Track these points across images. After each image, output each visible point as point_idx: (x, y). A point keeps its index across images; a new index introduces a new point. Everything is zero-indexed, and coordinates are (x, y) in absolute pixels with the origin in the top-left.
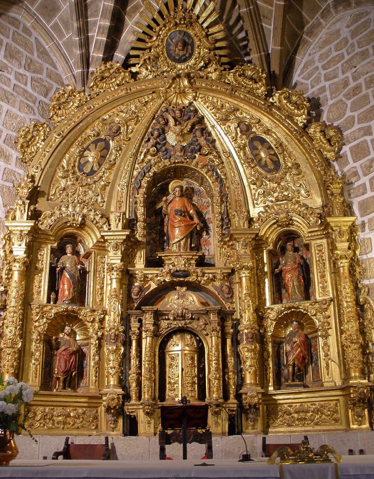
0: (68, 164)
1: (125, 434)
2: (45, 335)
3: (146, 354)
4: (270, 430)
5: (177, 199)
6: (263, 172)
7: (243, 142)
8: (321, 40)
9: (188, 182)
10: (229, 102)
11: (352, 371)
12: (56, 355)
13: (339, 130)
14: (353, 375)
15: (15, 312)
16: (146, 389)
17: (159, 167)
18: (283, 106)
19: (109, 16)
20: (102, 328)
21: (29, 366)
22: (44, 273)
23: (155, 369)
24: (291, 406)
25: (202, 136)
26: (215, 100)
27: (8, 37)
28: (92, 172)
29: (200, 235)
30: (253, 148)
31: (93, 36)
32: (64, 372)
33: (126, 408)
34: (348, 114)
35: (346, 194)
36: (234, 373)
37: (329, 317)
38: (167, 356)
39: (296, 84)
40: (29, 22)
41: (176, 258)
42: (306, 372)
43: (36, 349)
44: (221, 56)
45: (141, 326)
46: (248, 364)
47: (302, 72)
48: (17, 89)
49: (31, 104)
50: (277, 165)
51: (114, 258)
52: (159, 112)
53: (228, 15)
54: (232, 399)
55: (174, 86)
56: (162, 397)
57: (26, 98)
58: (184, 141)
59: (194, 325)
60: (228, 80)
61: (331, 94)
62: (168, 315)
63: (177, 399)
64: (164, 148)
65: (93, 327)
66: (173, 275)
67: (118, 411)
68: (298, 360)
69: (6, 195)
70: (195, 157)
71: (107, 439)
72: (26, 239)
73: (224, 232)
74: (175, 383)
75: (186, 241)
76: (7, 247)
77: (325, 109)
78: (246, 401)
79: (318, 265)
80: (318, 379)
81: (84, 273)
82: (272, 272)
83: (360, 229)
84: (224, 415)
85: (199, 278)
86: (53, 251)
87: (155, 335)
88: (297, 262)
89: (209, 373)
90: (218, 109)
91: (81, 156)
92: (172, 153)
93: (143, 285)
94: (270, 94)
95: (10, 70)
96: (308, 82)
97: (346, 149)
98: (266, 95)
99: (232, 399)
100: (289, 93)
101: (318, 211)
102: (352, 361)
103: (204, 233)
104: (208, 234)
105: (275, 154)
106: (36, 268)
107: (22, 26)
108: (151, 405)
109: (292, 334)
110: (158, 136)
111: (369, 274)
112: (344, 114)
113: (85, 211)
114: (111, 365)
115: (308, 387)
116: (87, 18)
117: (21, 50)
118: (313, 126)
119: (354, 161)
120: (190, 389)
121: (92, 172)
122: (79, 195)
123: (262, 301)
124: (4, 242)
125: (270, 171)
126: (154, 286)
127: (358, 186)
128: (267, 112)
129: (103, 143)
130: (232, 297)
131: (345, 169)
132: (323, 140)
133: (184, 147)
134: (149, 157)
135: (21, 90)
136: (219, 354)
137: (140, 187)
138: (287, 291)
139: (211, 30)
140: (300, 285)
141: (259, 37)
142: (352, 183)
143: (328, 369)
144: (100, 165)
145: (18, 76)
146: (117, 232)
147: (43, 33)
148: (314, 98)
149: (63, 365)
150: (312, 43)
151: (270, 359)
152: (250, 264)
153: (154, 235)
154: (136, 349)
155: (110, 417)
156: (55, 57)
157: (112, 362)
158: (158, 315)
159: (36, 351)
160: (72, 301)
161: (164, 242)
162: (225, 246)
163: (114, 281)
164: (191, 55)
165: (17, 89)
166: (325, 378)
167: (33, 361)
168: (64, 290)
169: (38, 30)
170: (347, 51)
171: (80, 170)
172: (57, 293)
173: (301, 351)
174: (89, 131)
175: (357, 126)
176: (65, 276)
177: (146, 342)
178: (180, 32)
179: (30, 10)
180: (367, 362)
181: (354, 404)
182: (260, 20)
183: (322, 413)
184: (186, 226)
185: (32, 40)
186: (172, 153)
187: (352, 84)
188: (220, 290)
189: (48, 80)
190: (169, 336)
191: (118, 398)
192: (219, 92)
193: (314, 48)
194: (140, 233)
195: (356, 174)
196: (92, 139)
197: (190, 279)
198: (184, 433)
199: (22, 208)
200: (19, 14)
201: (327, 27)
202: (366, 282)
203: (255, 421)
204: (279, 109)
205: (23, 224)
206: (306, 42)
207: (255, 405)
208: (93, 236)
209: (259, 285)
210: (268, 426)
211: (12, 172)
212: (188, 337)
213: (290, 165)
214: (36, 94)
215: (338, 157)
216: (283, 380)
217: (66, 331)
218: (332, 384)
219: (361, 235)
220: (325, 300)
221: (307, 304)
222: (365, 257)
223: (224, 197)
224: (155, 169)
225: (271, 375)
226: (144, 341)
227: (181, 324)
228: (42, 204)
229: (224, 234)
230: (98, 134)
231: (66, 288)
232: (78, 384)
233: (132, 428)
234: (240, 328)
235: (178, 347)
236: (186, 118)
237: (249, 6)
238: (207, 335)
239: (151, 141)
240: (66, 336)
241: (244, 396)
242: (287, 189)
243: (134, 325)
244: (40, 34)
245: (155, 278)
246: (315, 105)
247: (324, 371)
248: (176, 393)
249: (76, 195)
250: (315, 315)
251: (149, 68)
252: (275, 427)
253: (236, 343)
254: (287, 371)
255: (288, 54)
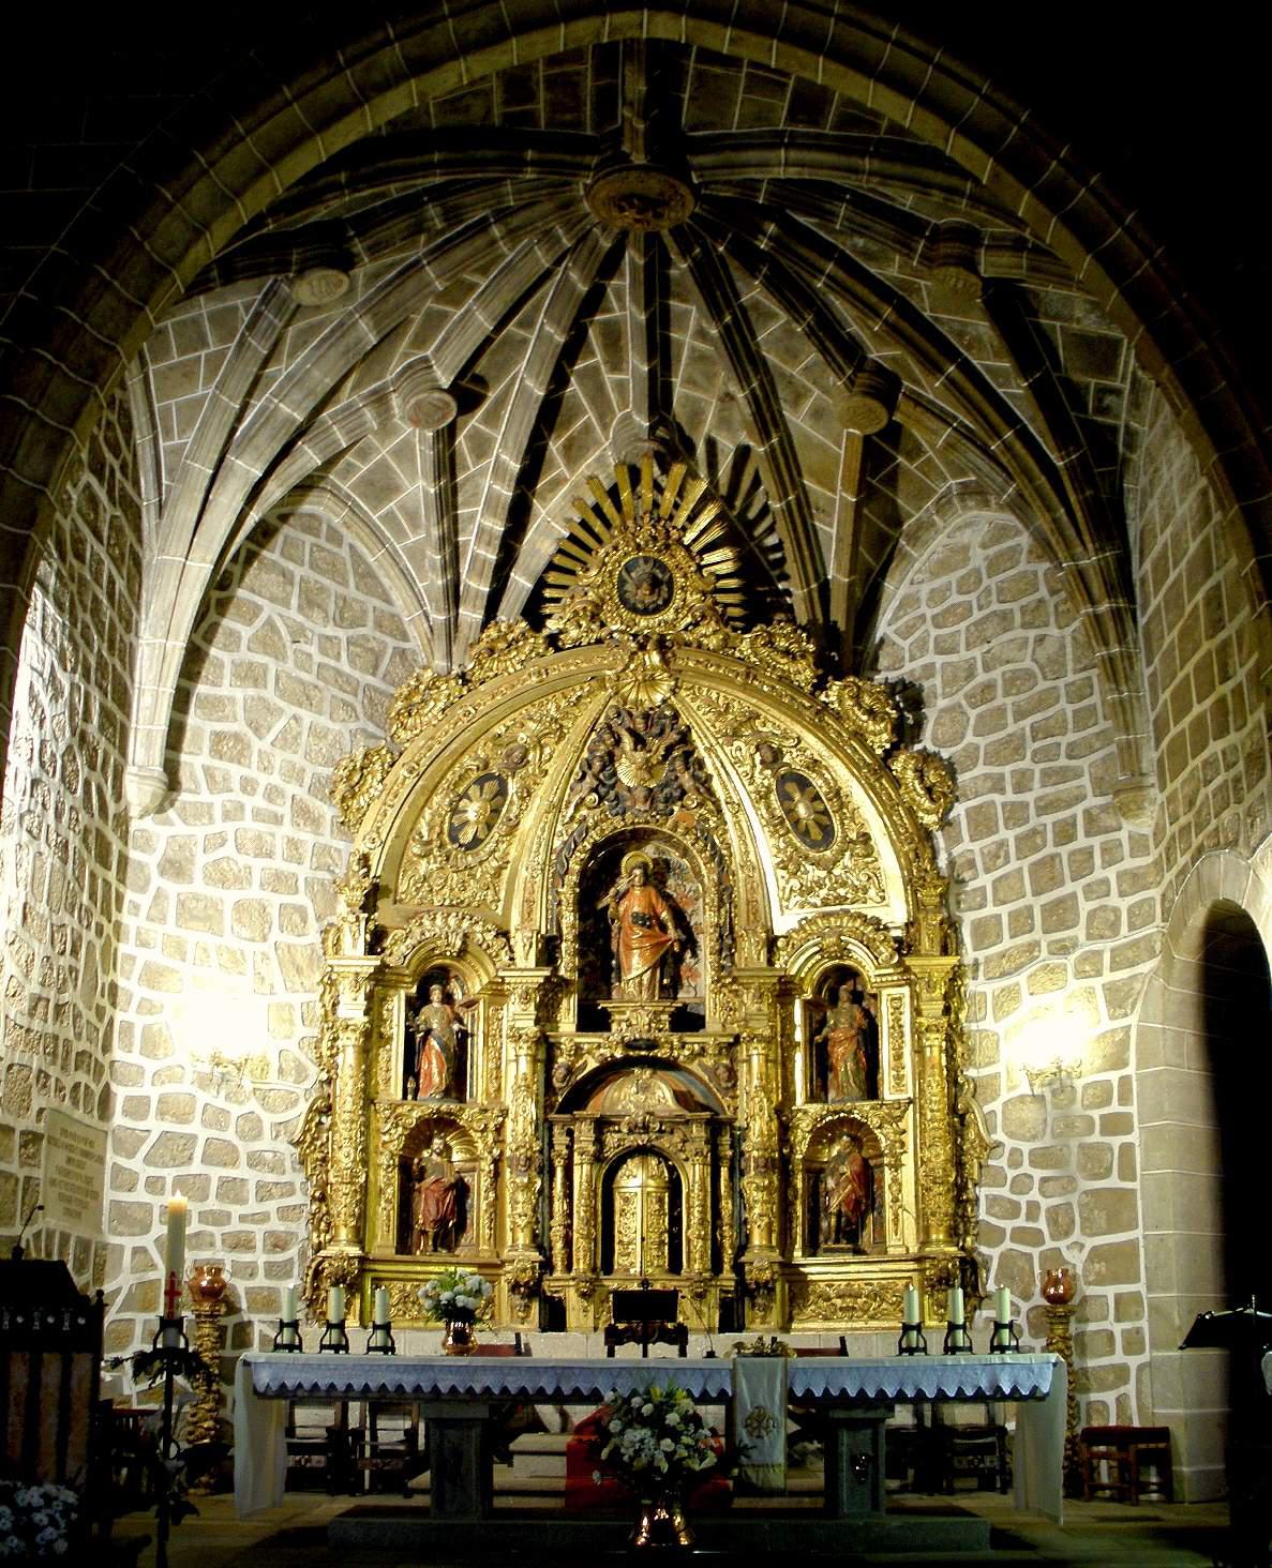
0: (431, 829)
1: (544, 1328)
2: (401, 1157)
3: (581, 1194)
4: (794, 1326)
5: (637, 891)
6: (804, 847)
7: (766, 783)
8: (935, 556)
9: (657, 848)
10: (743, 702)
11: (933, 1230)
12: (419, 1191)
13: (951, 770)
14: (934, 1237)
15: (352, 1122)
16: (581, 1254)
17: (602, 830)
18: (846, 712)
19: (504, 514)
20: (499, 1141)
21: (376, 1212)
22: (394, 1043)
23: (595, 1219)
24: (830, 1286)
25: (687, 769)
26: (714, 696)
27: (302, 564)
28: (476, 842)
29: (679, 959)
30: (785, 797)
31: (467, 543)
32: (435, 1222)
33: (545, 1285)
34: (970, 738)
35: (952, 900)
36: (731, 1227)
37: (904, 1132)
38: (617, 1196)
39: (882, 641)
40: (337, 516)
41: (635, 1011)
42: (863, 1227)
43: (387, 1181)
44: (726, 606)
45: (572, 1141)
46: (757, 1211)
47: (895, 618)
48: (326, 674)
49: (349, 698)
50: (827, 831)
51: (519, 1015)
52: (602, 720)
53: (745, 501)
54: (727, 1272)
55: (632, 666)
56: (608, 1267)
57: (341, 689)
58: (652, 777)
59: (665, 1143)
60: (741, 652)
61: (945, 684)
62: (619, 1124)
63: (632, 1271)
64: (612, 794)
65: (484, 1140)
66: (629, 1046)
67: (531, 1290)
68: (847, 1205)
69: (319, 896)
70: (672, 812)
71: (518, 1336)
72: (366, 987)
73: (723, 962)
74: (629, 1243)
75: (653, 975)
76: (327, 997)
77: (931, 713)
78: (751, 1276)
79: (891, 1035)
80: (880, 1239)
81: (464, 1037)
82: (810, 1041)
83: (970, 974)
84: (714, 1297)
85: (676, 1053)
86: (409, 1000)
87: (598, 1158)
88: (856, 1025)
89: (689, 1227)
90: (720, 714)
91: (455, 811)
92: (628, 804)
93: (573, 1063)
94: (820, 685)
95: (310, 635)
96: (906, 644)
97: (959, 810)
98: (814, 685)
99: (727, 1272)
100: (859, 688)
101: (898, 933)
102: (933, 1214)
103: (688, 954)
104: (694, 955)
105: (825, 812)
106: (381, 1035)
107: (324, 527)
108: (591, 1281)
109: (840, 1158)
110: (603, 769)
111: (978, 1058)
112: (962, 738)
113: (466, 924)
114: (519, 1210)
115: (862, 1253)
116: (455, 508)
117: (326, 582)
118: (902, 757)
119: (972, 840)
120: (655, 1253)
121: (476, 842)
122: (452, 890)
123: (789, 1097)
124: (321, 988)
125: (814, 845)
126: (592, 1064)
127: (974, 890)
128: (815, 725)
129: (496, 782)
130: (735, 1085)
131: (956, 851)
132: (918, 787)
133: (651, 790)
134: (584, 812)
135: (332, 673)
136: (705, 1196)
137: (566, 873)
138: (836, 1076)
139: (709, 558)
140: (858, 1068)
141: (806, 553)
142: (963, 882)
143: (896, 1225)
144: (489, 827)
145: (327, 642)
146: (526, 970)
147: (365, 532)
148: (912, 684)
149: (433, 1209)
150: (916, 560)
151: (798, 1202)
152: (767, 1033)
153: (591, 957)
154: (563, 1184)
155: (517, 1300)
156: (389, 580)
157: (518, 1208)
158: (602, 1125)
159: (388, 1185)
160: (447, 1093)
161: (612, 969)
162: (725, 990)
163: (523, 1060)
164: (667, 602)
165: (326, 674)
166: (891, 1239)
167: (383, 1204)
168: (429, 1075)
169: (355, 527)
170: (978, 599)
171: (454, 839)
172: (417, 1077)
173: (853, 1191)
174: (467, 761)
175: (981, 769)
176: (431, 1048)
177: (580, 1174)
178: (646, 560)
179: (339, 489)
180: (963, 1216)
181: (933, 1286)
182: (811, 515)
183: (883, 1300)
184: (652, 946)
185: (344, 552)
186: (628, 804)
187: (981, 677)
188: (713, 1072)
189: (378, 635)
190: (621, 1160)
191: (533, 1268)
192: (723, 679)
193: (919, 571)
194: (567, 965)
195: (971, 864)
196: (474, 775)
197: (661, 1053)
198: (645, 1328)
199: (354, 928)
200: (319, 504)
201: (947, 531)
202: (971, 1073)
203: (767, 1309)
204: (838, 717)
205: (355, 959)
206: (905, 555)
207: (767, 1282)
208: (481, 972)
209: (784, 1065)
210: (791, 1319)
211: (326, 849)
212: (654, 1162)
213: (853, 836)
214: (357, 674)
215: (945, 823)
216: (822, 1238)
217: (435, 1147)
218: (902, 1251)
219: (971, 986)
220: (898, 1101)
221: (867, 1105)
222: (974, 1026)
223: (725, 893)
224: (595, 836)
225: (799, 1230)
226: (577, 1170)
227: (642, 1139)
228: (385, 913)
229: (723, 968)
230: (486, 766)
231: (433, 1067)
232: (457, 1241)
233: (554, 1318)
234: (745, 1147)
235: (636, 1180)
236: (656, 730)
237: (786, 495)
238: (687, 1160)
239: (588, 779)
240: (434, 1156)
241: (747, 1268)
242: (844, 884)
243: (560, 1140)
244: (357, 535)
245: (597, 1049)
246: (909, 699)
247: (889, 1226)
248: (632, 1259)
249: (446, 890)
250: (880, 1127)
251: (583, 623)
252: (802, 1321)
253: (737, 1172)
254: (828, 1224)
255: (869, 575)
